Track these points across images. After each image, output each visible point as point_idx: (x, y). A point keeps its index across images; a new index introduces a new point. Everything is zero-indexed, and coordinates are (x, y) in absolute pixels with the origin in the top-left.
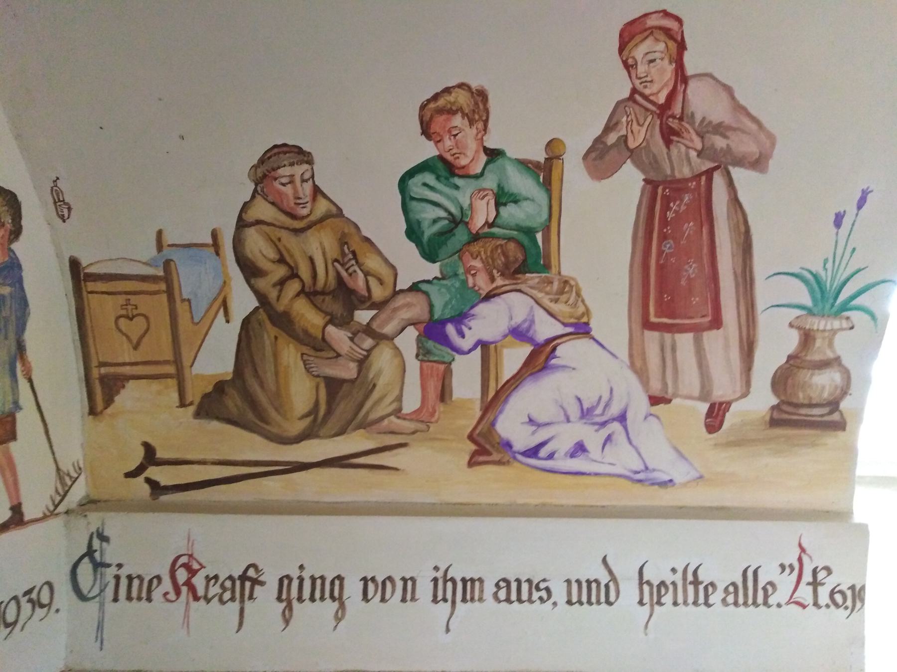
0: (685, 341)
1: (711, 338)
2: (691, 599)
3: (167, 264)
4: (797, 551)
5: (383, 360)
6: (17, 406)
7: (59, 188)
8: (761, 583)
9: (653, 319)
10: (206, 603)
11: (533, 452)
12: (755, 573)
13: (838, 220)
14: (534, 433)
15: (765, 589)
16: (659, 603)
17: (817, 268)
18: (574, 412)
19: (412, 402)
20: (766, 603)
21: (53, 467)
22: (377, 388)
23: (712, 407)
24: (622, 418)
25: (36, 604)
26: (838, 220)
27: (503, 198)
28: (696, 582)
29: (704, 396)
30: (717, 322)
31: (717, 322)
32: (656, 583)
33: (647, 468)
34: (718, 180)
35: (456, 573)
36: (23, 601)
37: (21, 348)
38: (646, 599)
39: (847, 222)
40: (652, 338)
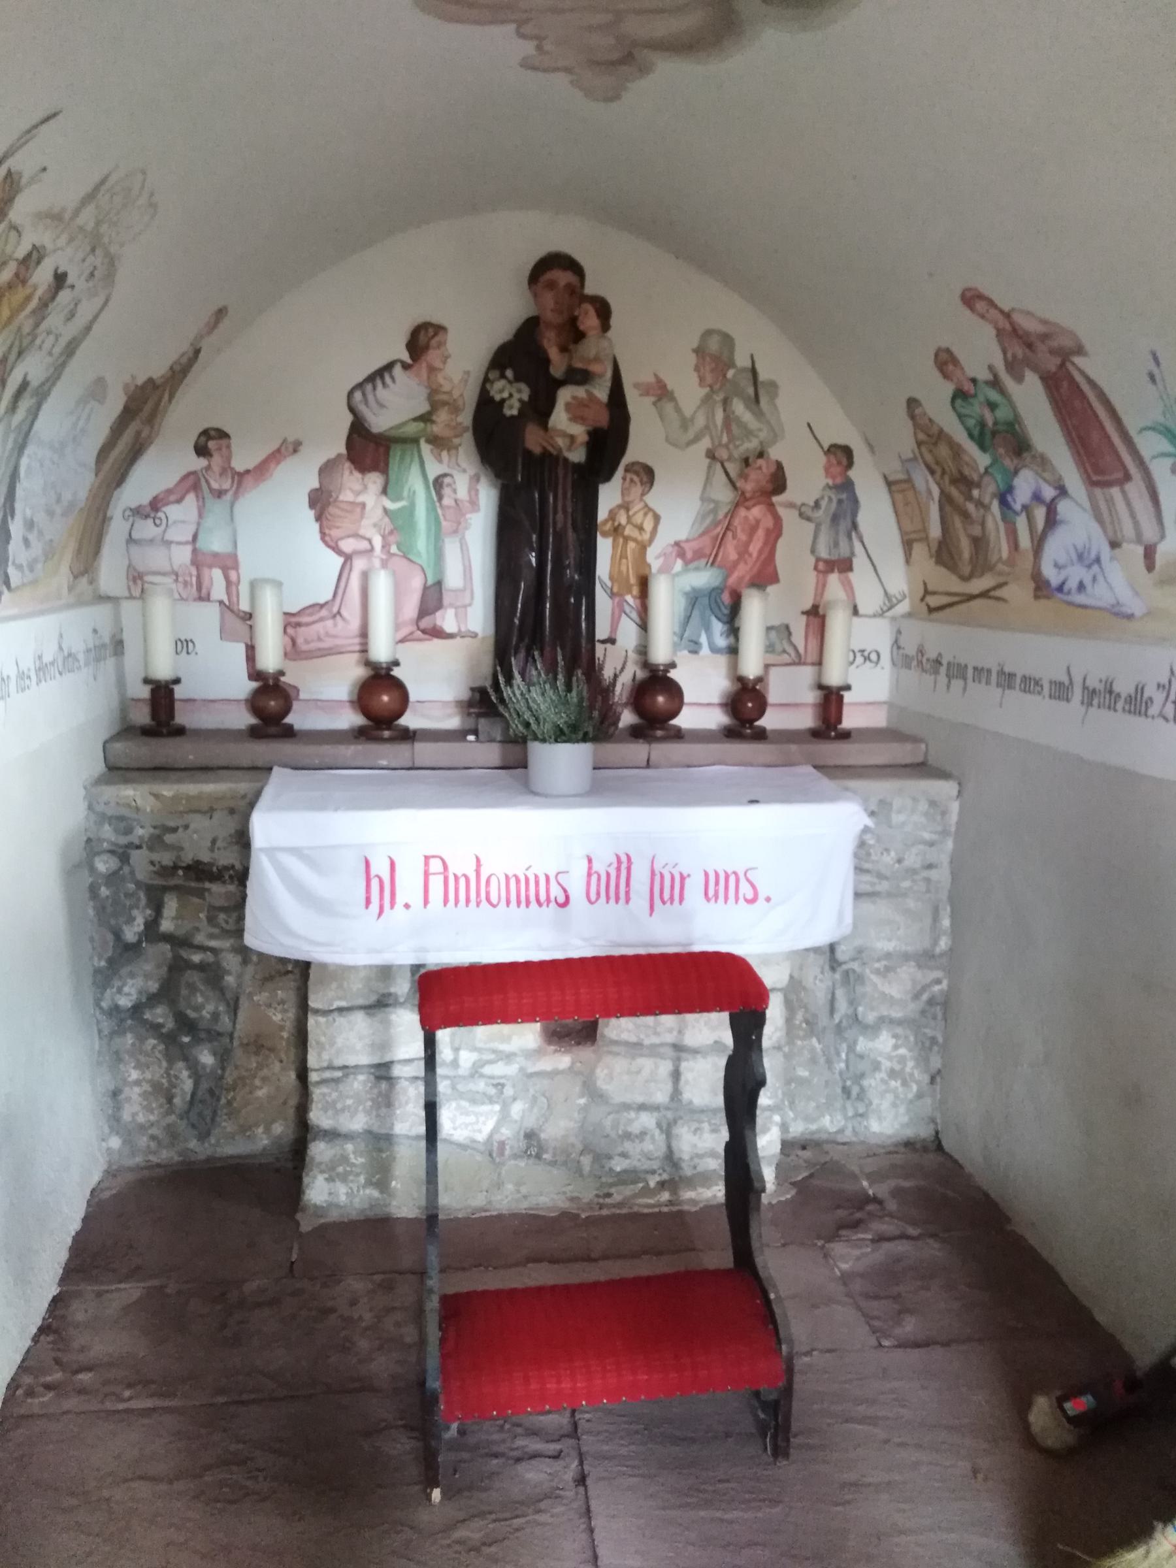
0: (1115, 491)
1: (1128, 487)
2: (1107, 704)
3: (908, 472)
4: (1168, 673)
5: (990, 524)
6: (853, 554)
7: (1161, 372)
8: (1146, 695)
9: (1095, 478)
10: (13, 170)
11: (1060, 588)
12: (1142, 689)
13: (1152, 377)
14: (1059, 573)
15: (1146, 703)
16: (1091, 705)
17: (1161, 419)
18: (1074, 557)
19: (1005, 554)
20: (1146, 715)
21: (882, 592)
22: (322, 460)
23: (1146, 549)
24: (1098, 560)
25: (867, 659)
26: (1152, 377)
27: (992, 406)
28: (1111, 692)
29: (1139, 539)
30: (1127, 477)
31: (1127, 477)
32: (1091, 688)
33: (1118, 603)
34: (1069, 365)
35: (1007, 670)
36: (858, 655)
37: (855, 526)
38: (1086, 701)
39: (1158, 378)
40: (1098, 492)
